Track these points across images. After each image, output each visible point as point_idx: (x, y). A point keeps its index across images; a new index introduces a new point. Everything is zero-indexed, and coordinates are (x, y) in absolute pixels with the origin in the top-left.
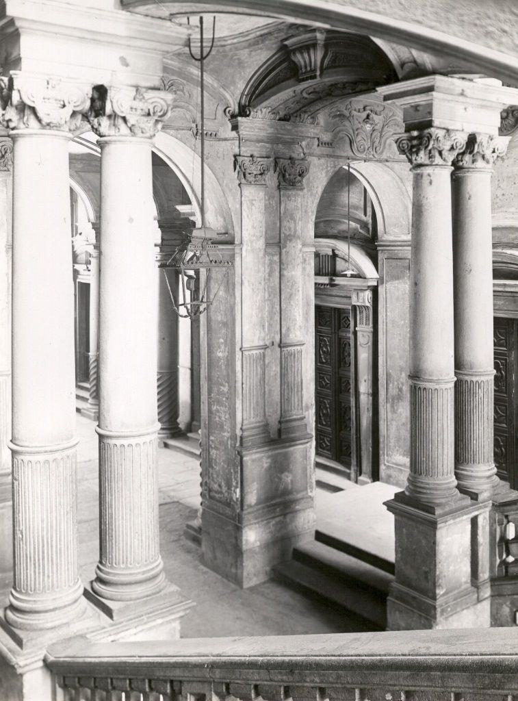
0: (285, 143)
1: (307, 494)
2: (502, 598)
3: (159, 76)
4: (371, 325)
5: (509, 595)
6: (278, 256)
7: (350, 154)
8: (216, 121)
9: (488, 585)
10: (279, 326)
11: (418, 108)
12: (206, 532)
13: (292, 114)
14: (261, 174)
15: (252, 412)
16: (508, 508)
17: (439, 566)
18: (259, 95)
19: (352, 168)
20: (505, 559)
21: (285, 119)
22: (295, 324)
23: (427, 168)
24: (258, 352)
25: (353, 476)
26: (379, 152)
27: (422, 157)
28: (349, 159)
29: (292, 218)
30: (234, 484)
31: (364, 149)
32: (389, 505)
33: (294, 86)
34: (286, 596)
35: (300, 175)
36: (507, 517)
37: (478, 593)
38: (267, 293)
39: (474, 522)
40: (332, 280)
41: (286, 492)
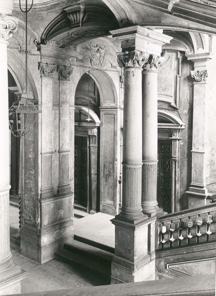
0: (62, 59)
1: (70, 219)
2: (160, 258)
3: (11, 9)
4: (97, 144)
5: (163, 257)
6: (58, 111)
7: (90, 66)
8: (30, 45)
9: (155, 253)
10: (58, 143)
11: (129, 41)
12: (23, 239)
13: (66, 45)
14: (51, 72)
15: (46, 182)
16: (164, 219)
17: (135, 247)
18: (50, 35)
19: (91, 74)
20: (161, 242)
21: (63, 47)
22: (66, 142)
23: (132, 68)
24: (49, 155)
25: (88, 210)
26: (103, 66)
27: (130, 63)
28: (90, 68)
29: (65, 93)
30: (37, 216)
31: (97, 64)
32: (113, 221)
33: (68, 30)
34: (62, 266)
35: (69, 74)
36: (163, 223)
37: (150, 257)
38: (53, 128)
39: (149, 226)
40: (79, 124)
41: (61, 219)
